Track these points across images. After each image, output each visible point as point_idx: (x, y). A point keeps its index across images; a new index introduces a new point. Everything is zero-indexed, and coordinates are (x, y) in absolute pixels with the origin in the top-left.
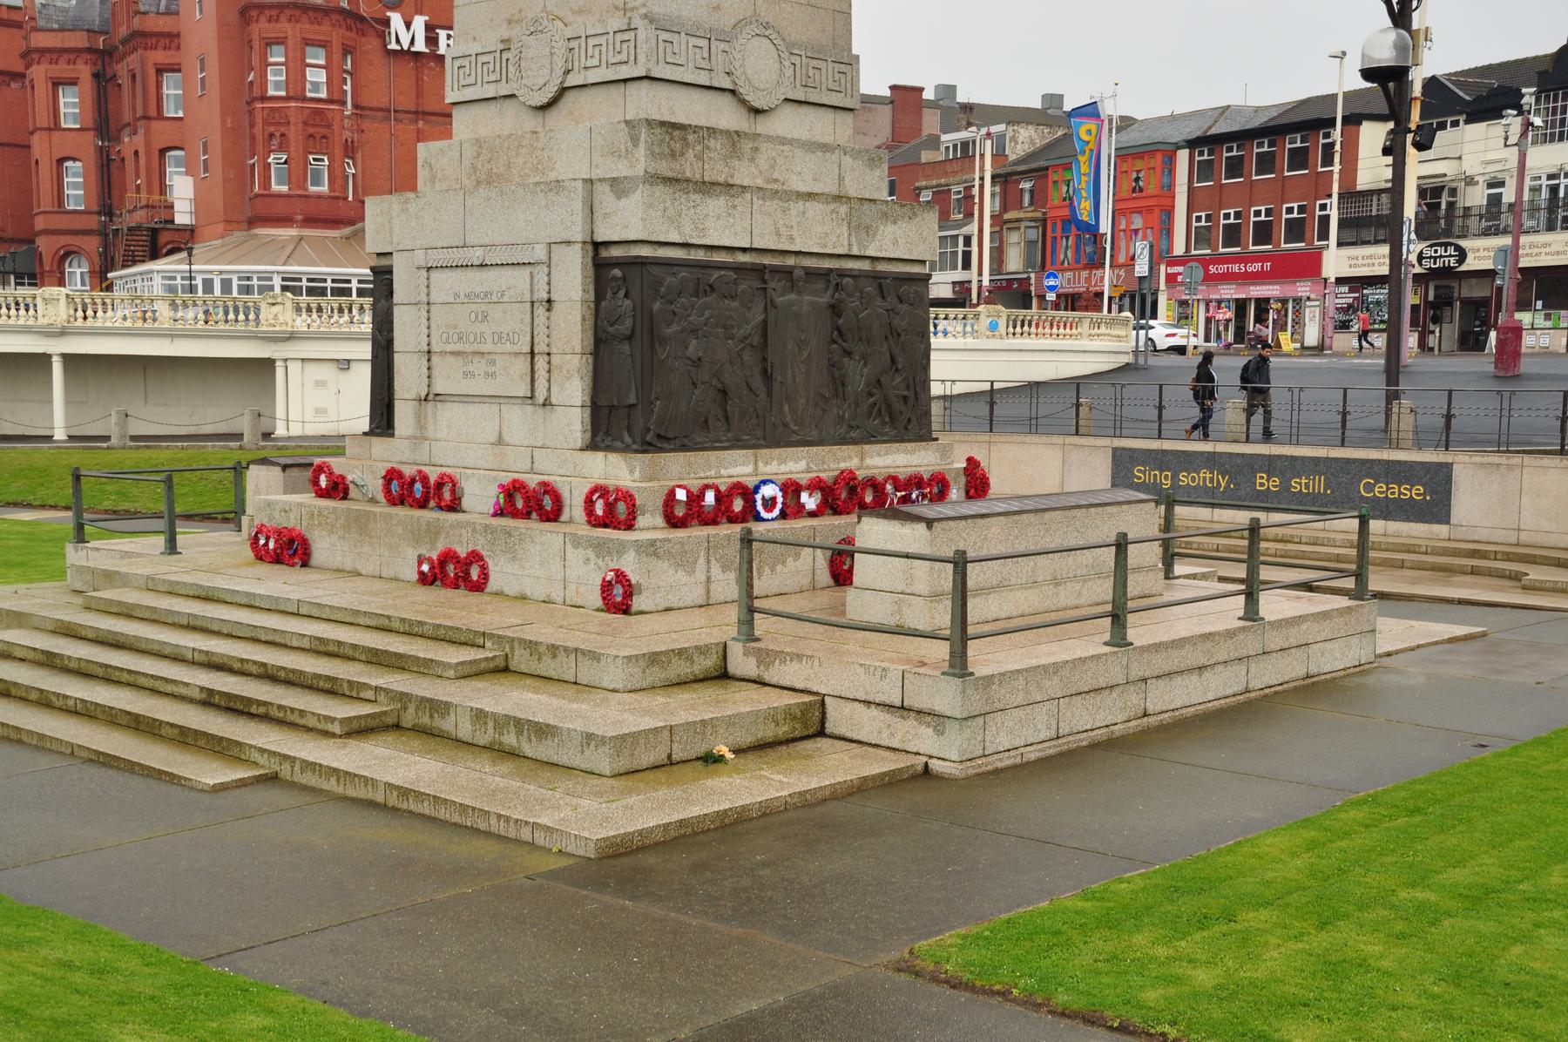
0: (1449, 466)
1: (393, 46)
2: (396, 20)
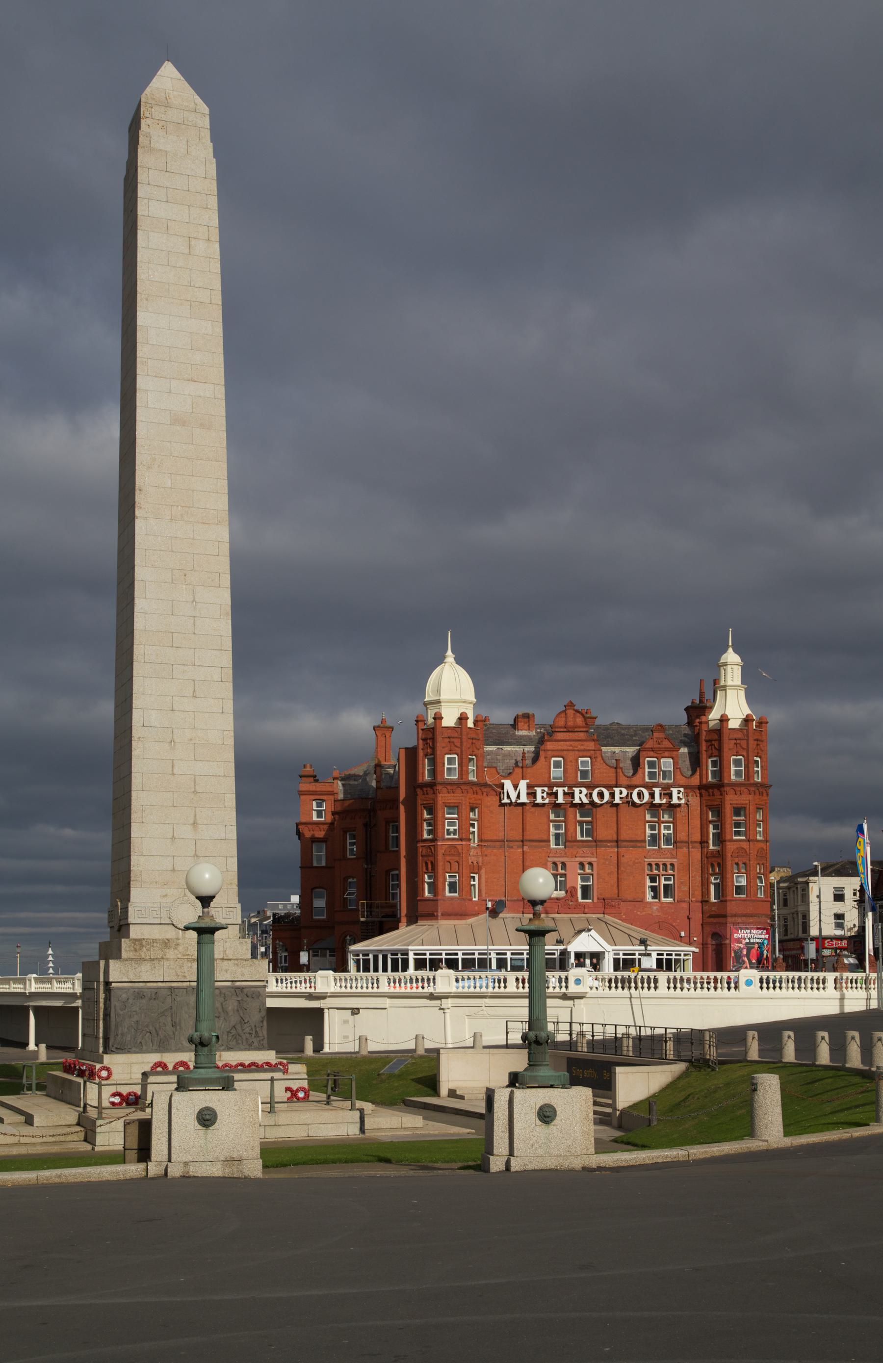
0: (786, 1134)
1: (506, 801)
2: (508, 784)
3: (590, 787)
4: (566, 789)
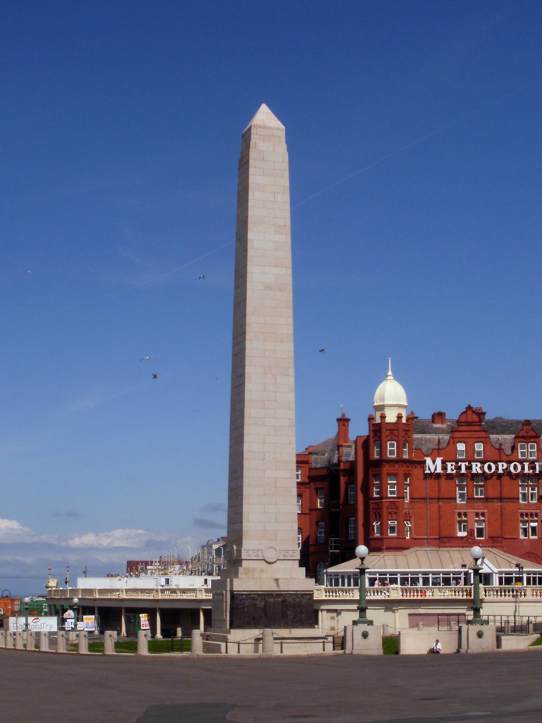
1: (427, 471)
2: (429, 461)
3: (483, 462)
4: (467, 464)
